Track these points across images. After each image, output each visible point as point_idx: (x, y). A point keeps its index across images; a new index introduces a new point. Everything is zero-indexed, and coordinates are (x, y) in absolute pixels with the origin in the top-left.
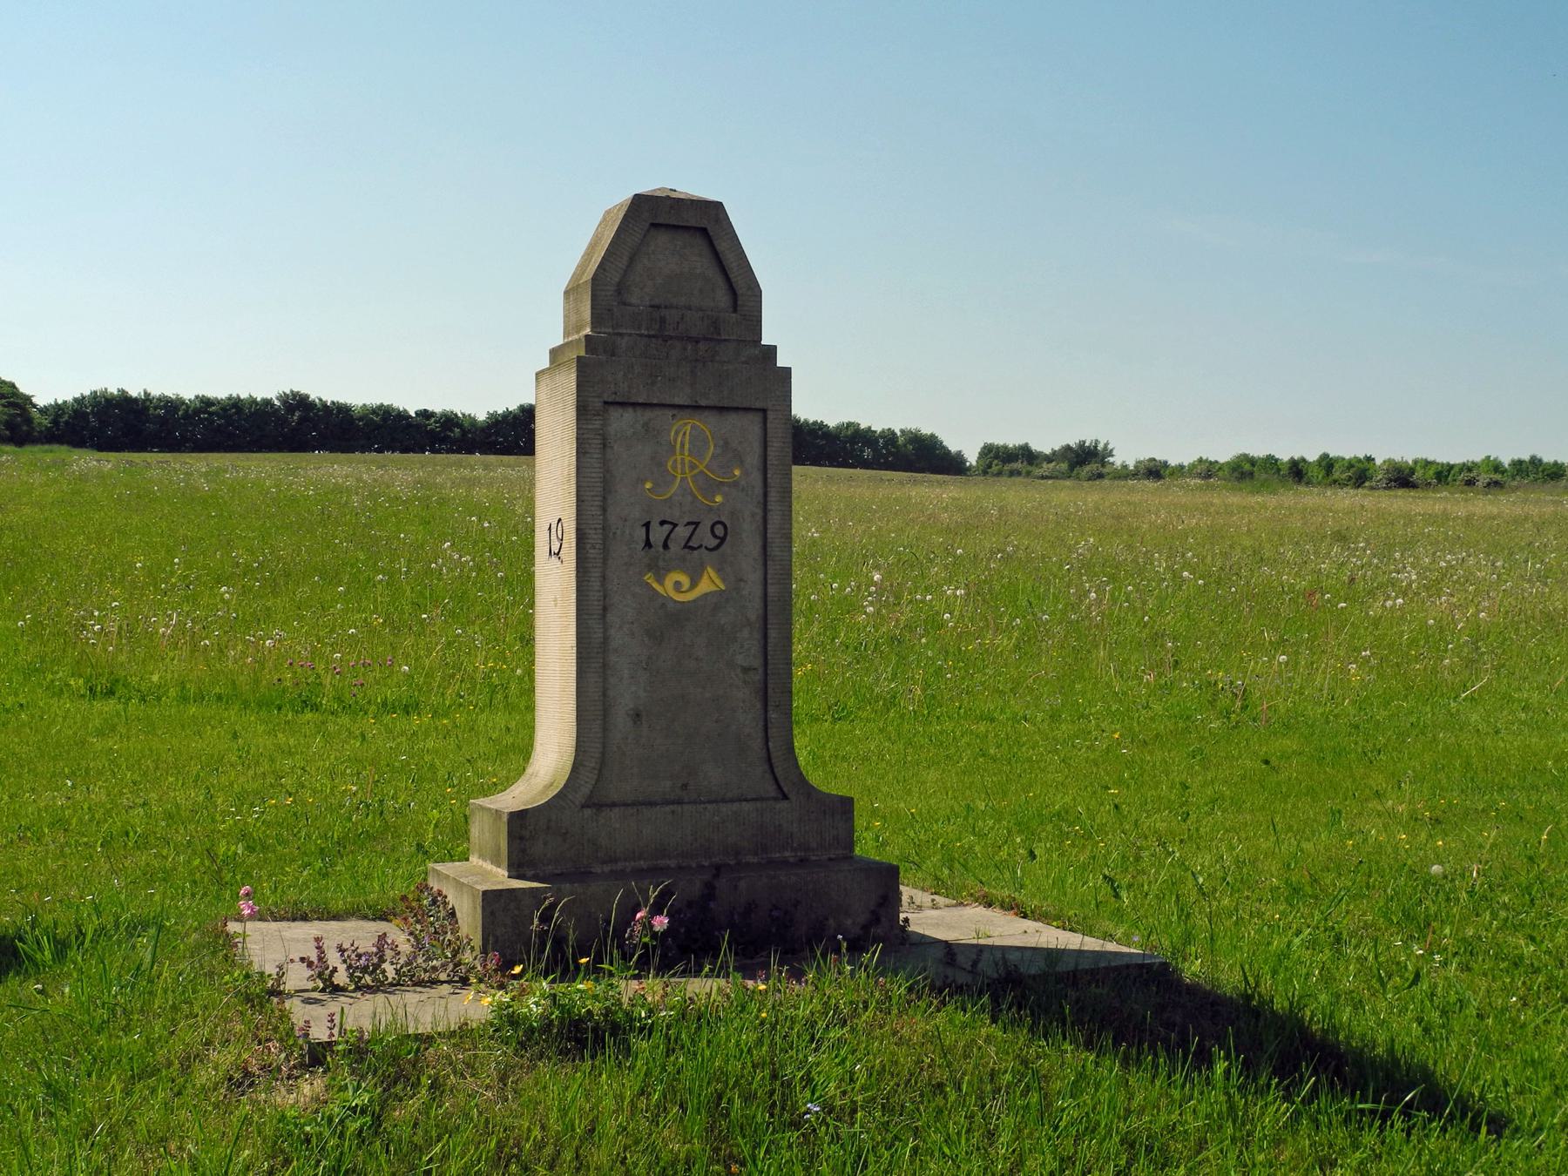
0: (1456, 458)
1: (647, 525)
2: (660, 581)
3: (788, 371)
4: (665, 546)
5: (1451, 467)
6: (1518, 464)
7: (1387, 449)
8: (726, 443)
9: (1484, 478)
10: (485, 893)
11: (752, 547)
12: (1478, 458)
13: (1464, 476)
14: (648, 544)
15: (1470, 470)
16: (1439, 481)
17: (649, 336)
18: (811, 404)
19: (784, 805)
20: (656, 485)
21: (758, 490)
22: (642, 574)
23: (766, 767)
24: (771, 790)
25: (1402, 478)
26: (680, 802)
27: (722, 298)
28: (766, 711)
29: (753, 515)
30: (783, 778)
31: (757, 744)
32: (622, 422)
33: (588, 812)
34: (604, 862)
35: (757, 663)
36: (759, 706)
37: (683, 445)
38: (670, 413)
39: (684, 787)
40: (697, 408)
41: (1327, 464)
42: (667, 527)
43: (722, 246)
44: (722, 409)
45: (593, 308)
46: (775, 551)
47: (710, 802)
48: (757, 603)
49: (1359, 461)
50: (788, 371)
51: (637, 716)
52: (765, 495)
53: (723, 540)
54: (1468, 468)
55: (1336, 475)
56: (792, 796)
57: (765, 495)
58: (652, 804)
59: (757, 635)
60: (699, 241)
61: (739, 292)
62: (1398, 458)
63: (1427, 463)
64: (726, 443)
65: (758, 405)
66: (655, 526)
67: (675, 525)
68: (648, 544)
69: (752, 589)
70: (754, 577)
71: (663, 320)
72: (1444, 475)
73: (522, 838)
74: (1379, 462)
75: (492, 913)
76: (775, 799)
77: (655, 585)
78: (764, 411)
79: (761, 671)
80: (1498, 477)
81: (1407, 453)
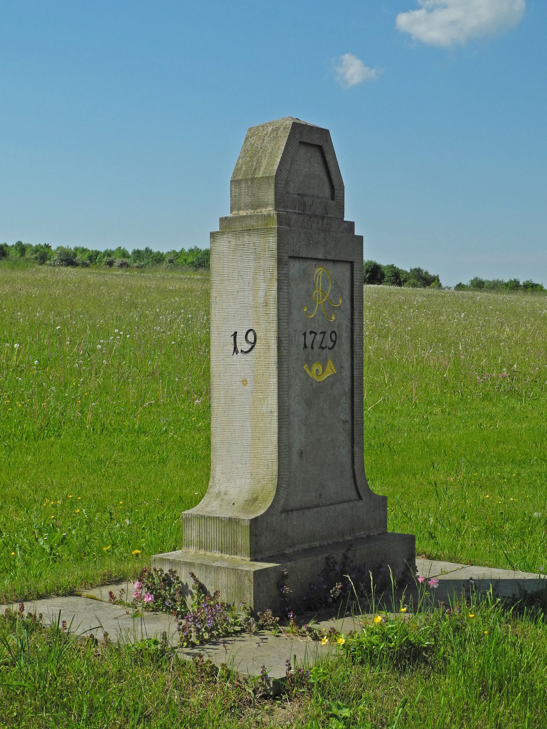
0: (164, 250)
1: (305, 334)
2: (310, 369)
3: (361, 238)
4: (312, 348)
5: (97, 253)
6: (138, 254)
7: (58, 241)
8: (336, 283)
9: (118, 261)
10: (255, 572)
11: (346, 347)
12: (113, 248)
13: (106, 259)
14: (305, 346)
15: (109, 255)
16: (91, 262)
17: (299, 214)
18: (370, 255)
19: (360, 503)
20: (308, 309)
21: (349, 312)
22: (303, 365)
23: (352, 480)
24: (358, 498)
25: (69, 259)
26: (318, 506)
27: (327, 192)
28: (353, 447)
29: (347, 327)
30: (360, 489)
31: (348, 467)
32: (295, 267)
33: (283, 516)
34: (290, 547)
35: (348, 418)
36: (349, 443)
37: (319, 281)
38: (314, 263)
39: (320, 495)
40: (325, 260)
41: (22, 248)
42: (313, 335)
43: (329, 158)
44: (335, 261)
45: (276, 195)
46: (356, 349)
47: (332, 504)
48: (348, 381)
49: (41, 247)
50: (361, 238)
51: (301, 454)
52: (352, 314)
53: (335, 342)
54: (108, 254)
55: (28, 255)
56: (364, 498)
57: (352, 314)
58: (309, 508)
59: (349, 401)
60: (318, 155)
61: (335, 187)
62: (65, 246)
63: (84, 250)
64: (336, 283)
65: (350, 260)
66: (308, 333)
67: (316, 334)
68: (305, 346)
69: (346, 373)
70: (347, 365)
71: (305, 204)
72: (93, 258)
73: (256, 535)
74: (54, 248)
75: (258, 585)
76: (355, 500)
77: (308, 371)
78: (352, 263)
79: (350, 422)
80: (125, 260)
81: (71, 244)
